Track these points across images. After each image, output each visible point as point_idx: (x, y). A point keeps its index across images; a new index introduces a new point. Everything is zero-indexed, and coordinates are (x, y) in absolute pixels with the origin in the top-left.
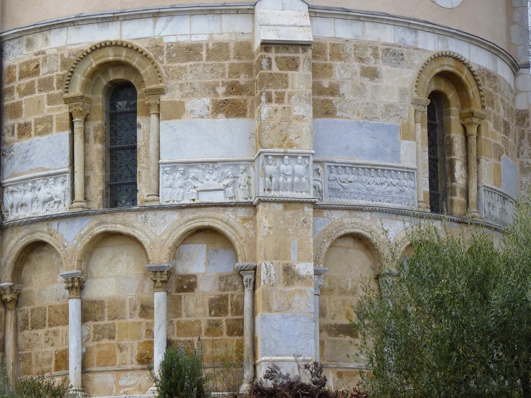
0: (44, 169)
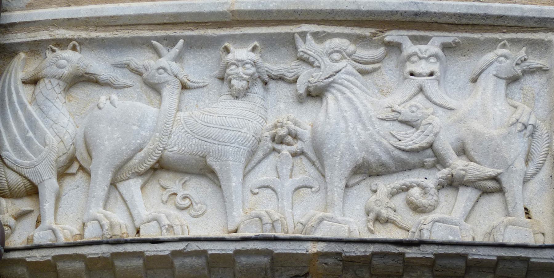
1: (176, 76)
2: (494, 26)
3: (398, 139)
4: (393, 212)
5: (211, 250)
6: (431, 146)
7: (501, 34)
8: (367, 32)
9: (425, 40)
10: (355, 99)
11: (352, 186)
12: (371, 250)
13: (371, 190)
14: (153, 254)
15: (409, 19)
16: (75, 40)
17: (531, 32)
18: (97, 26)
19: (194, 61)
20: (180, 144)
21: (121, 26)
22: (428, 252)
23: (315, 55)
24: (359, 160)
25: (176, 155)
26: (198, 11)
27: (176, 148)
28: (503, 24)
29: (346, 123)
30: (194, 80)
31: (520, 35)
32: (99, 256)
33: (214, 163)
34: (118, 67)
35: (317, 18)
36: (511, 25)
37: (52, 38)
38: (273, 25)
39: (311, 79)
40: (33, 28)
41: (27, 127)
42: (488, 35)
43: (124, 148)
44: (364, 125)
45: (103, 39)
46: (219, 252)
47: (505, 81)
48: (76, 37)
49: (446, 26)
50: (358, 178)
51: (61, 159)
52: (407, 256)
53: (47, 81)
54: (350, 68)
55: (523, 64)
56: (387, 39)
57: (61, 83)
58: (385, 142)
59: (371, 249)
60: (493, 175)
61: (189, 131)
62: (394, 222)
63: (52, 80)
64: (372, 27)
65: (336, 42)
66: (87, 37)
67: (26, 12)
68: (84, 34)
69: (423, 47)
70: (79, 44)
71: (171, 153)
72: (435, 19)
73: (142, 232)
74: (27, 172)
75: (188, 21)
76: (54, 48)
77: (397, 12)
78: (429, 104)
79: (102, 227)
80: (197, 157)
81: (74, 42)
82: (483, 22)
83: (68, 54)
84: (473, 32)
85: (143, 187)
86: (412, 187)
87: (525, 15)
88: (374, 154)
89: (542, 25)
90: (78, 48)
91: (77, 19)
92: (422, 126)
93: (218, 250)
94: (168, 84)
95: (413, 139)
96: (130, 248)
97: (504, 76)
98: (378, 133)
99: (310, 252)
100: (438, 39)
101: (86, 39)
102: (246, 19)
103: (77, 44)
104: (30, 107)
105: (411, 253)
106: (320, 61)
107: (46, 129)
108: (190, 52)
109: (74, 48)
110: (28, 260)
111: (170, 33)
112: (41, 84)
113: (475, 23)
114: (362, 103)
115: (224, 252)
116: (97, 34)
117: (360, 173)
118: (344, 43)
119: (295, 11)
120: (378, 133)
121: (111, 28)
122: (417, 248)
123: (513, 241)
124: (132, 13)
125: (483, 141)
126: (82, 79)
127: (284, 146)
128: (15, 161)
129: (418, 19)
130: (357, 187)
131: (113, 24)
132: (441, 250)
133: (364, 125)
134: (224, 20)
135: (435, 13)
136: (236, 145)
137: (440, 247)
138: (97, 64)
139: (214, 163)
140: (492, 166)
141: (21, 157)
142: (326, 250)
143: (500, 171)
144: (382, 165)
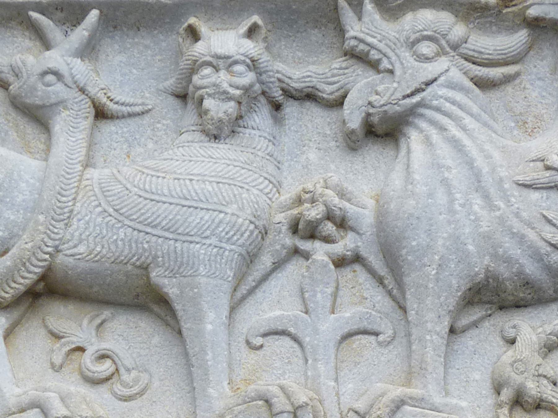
1: (82, 90)
4: (550, 387)
23: (381, 46)
24: (477, 274)
25: (82, 264)
33: (166, 281)
39: (374, 98)
54: (455, 75)
58: (531, 235)
71: (71, 259)
88: (508, 260)
98: (517, 215)
106: (394, 58)
114: (482, 150)
120: (517, 215)
127: (318, 244)
130: (474, 332)
133: (486, 197)
139: (166, 281)
144: (527, 284)
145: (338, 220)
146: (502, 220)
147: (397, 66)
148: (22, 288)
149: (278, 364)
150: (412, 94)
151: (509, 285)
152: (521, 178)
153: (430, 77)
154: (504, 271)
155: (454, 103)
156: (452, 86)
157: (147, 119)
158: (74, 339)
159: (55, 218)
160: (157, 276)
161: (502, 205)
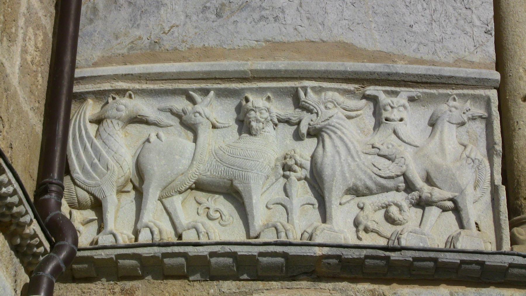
0: (350, 51)
1: (208, 119)
2: (445, 84)
3: (378, 169)
4: (376, 225)
5: (240, 252)
6: (404, 175)
7: (451, 91)
8: (351, 87)
9: (395, 94)
10: (345, 138)
11: (345, 203)
12: (364, 254)
13: (358, 207)
14: (194, 254)
15: (383, 78)
16: (130, 90)
17: (472, 89)
18: (147, 80)
19: (220, 108)
20: (212, 171)
21: (166, 80)
22: (409, 255)
23: (313, 104)
24: (350, 184)
25: (209, 179)
26: (225, 69)
27: (209, 173)
28: (453, 82)
29: (340, 156)
30: (220, 121)
31: (465, 91)
32: (151, 255)
33: (239, 185)
34: (162, 111)
35: (315, 76)
36: (459, 83)
37: (113, 88)
38: (281, 81)
39: (312, 123)
40: (98, 81)
41: (94, 156)
42: (441, 91)
43: (169, 172)
44: (352, 157)
45: (151, 90)
46: (246, 254)
47: (455, 125)
48: (131, 88)
49: (411, 83)
50: (349, 197)
51: (120, 180)
52: (392, 258)
53: (109, 121)
54: (340, 115)
55: (467, 113)
56: (368, 93)
57: (120, 123)
58: (369, 171)
59: (364, 252)
60: (451, 197)
61: (219, 160)
62: (378, 233)
63: (113, 120)
64: (356, 83)
65: (330, 94)
66: (140, 88)
67: (93, 69)
68: (137, 86)
69: (395, 100)
70: (134, 93)
71: (205, 177)
72: (402, 78)
73: (184, 237)
74: (93, 190)
75: (217, 77)
76: (114, 96)
77: (374, 73)
78: (400, 142)
79: (152, 233)
80: (225, 180)
81: (130, 92)
82: (437, 81)
83: (125, 101)
84: (430, 88)
85: (183, 202)
86: (390, 205)
87: (469, 76)
88: (361, 180)
89: (481, 84)
90: (133, 96)
91: (132, 75)
92: (396, 159)
93: (246, 252)
94: (202, 125)
95: (388, 168)
96: (176, 249)
97: (454, 122)
98: (364, 164)
99: (317, 255)
100: (405, 93)
101: (139, 90)
102: (261, 76)
103: (132, 93)
104: (95, 141)
105: (394, 256)
106: (318, 108)
107: (108, 157)
108: (218, 101)
109: (130, 97)
110: (96, 257)
111: (203, 85)
112: (105, 123)
113: (432, 81)
114: (350, 141)
115: (250, 254)
116: (147, 86)
117: (350, 194)
118: (337, 96)
119: (298, 71)
120: (364, 164)
121: (158, 82)
122: (399, 252)
123: (469, 248)
124: (175, 71)
125: (442, 171)
126: (138, 120)
127: (292, 173)
128: (84, 181)
129: (390, 78)
130: (347, 204)
131: (160, 78)
132: (417, 254)
133: (352, 157)
134: (244, 77)
135: (403, 74)
136: (255, 171)
137: (417, 252)
138: (146, 107)
139: (239, 185)
140: (450, 190)
141: (88, 179)
142: (330, 253)
143: (457, 194)
144: (367, 188)
145: (299, 165)
146: (358, 165)
147: (319, 111)
148: (188, 187)
149: (277, 214)
150: (325, 121)
151: (361, 189)
152: (364, 151)
153: (331, 115)
154: (359, 184)
155: (339, 124)
156: (339, 118)
157: (230, 128)
158: (206, 204)
159: (299, 162)
160: (236, 183)
161: (358, 160)
